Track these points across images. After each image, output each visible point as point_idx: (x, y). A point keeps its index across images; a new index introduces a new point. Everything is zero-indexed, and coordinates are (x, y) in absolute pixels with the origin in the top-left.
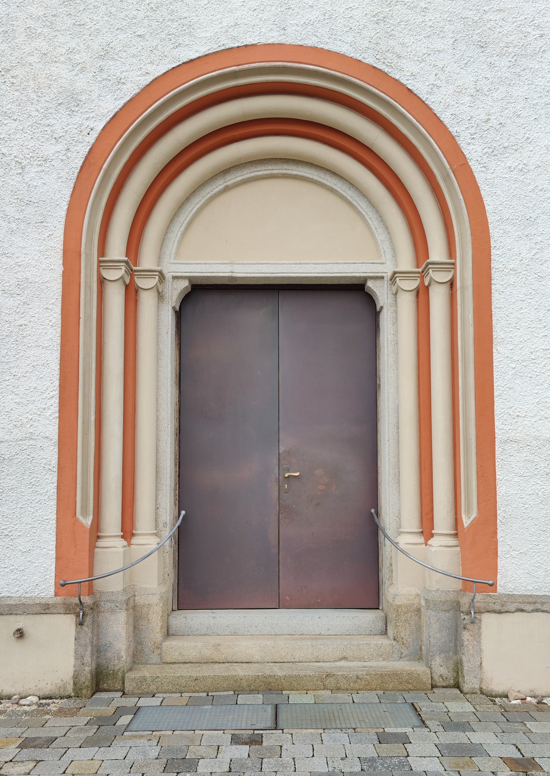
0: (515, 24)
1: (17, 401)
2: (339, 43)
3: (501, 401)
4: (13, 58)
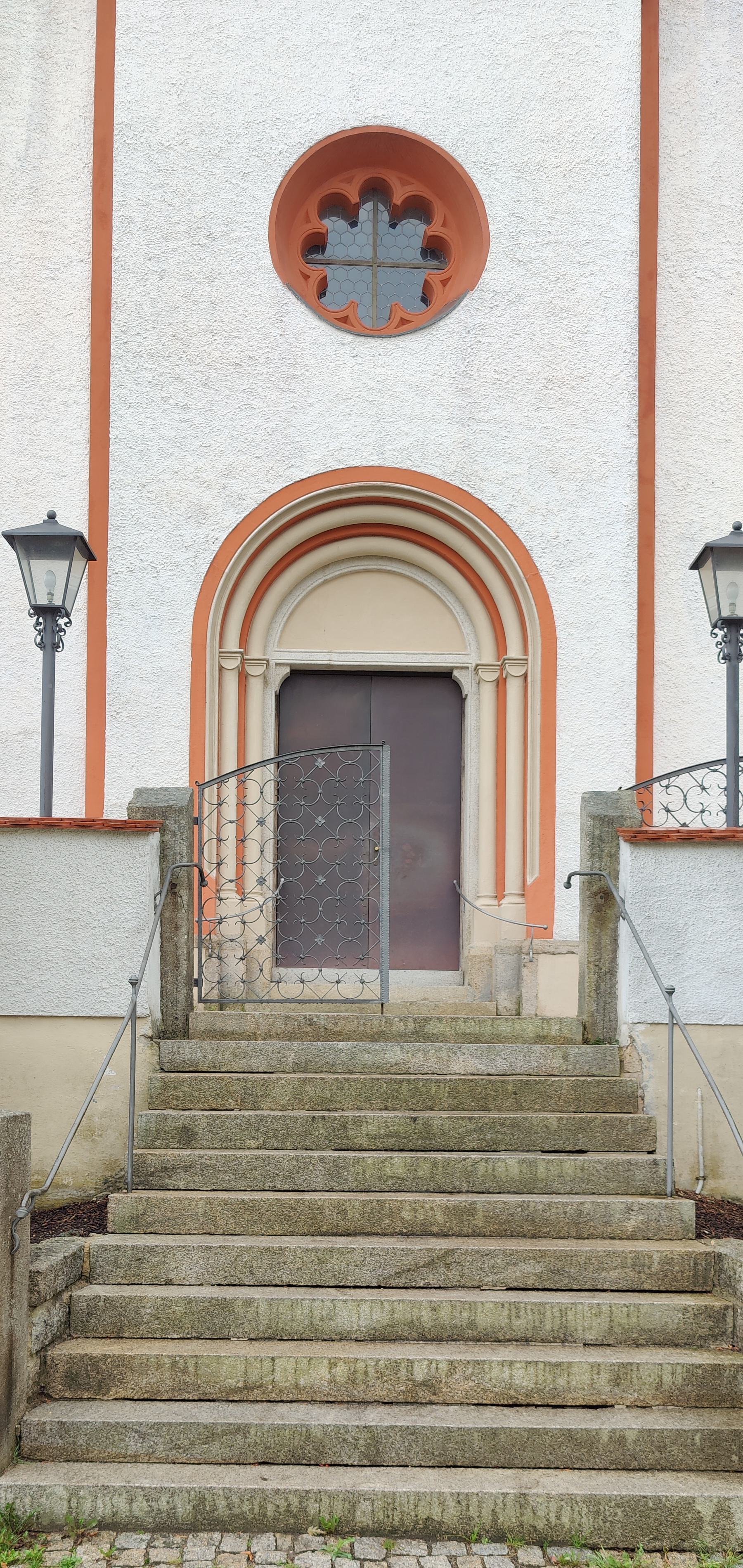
0: (583, 452)
1: (154, 772)
2: (430, 467)
3: (561, 779)
4: (149, 475)
